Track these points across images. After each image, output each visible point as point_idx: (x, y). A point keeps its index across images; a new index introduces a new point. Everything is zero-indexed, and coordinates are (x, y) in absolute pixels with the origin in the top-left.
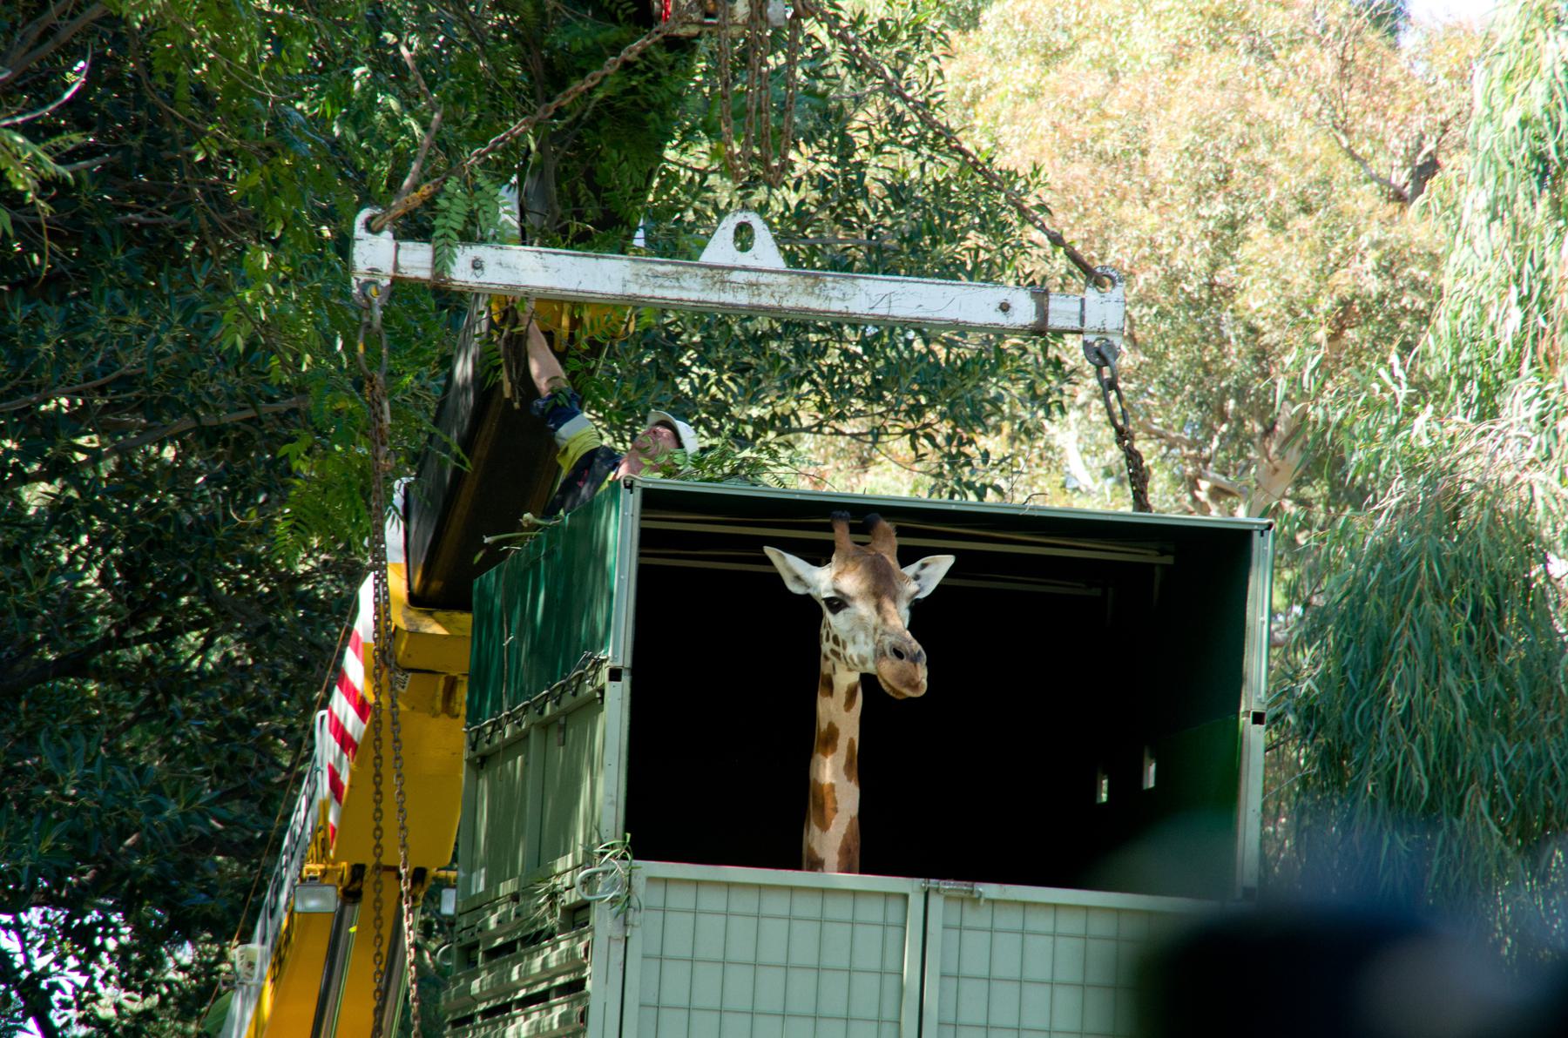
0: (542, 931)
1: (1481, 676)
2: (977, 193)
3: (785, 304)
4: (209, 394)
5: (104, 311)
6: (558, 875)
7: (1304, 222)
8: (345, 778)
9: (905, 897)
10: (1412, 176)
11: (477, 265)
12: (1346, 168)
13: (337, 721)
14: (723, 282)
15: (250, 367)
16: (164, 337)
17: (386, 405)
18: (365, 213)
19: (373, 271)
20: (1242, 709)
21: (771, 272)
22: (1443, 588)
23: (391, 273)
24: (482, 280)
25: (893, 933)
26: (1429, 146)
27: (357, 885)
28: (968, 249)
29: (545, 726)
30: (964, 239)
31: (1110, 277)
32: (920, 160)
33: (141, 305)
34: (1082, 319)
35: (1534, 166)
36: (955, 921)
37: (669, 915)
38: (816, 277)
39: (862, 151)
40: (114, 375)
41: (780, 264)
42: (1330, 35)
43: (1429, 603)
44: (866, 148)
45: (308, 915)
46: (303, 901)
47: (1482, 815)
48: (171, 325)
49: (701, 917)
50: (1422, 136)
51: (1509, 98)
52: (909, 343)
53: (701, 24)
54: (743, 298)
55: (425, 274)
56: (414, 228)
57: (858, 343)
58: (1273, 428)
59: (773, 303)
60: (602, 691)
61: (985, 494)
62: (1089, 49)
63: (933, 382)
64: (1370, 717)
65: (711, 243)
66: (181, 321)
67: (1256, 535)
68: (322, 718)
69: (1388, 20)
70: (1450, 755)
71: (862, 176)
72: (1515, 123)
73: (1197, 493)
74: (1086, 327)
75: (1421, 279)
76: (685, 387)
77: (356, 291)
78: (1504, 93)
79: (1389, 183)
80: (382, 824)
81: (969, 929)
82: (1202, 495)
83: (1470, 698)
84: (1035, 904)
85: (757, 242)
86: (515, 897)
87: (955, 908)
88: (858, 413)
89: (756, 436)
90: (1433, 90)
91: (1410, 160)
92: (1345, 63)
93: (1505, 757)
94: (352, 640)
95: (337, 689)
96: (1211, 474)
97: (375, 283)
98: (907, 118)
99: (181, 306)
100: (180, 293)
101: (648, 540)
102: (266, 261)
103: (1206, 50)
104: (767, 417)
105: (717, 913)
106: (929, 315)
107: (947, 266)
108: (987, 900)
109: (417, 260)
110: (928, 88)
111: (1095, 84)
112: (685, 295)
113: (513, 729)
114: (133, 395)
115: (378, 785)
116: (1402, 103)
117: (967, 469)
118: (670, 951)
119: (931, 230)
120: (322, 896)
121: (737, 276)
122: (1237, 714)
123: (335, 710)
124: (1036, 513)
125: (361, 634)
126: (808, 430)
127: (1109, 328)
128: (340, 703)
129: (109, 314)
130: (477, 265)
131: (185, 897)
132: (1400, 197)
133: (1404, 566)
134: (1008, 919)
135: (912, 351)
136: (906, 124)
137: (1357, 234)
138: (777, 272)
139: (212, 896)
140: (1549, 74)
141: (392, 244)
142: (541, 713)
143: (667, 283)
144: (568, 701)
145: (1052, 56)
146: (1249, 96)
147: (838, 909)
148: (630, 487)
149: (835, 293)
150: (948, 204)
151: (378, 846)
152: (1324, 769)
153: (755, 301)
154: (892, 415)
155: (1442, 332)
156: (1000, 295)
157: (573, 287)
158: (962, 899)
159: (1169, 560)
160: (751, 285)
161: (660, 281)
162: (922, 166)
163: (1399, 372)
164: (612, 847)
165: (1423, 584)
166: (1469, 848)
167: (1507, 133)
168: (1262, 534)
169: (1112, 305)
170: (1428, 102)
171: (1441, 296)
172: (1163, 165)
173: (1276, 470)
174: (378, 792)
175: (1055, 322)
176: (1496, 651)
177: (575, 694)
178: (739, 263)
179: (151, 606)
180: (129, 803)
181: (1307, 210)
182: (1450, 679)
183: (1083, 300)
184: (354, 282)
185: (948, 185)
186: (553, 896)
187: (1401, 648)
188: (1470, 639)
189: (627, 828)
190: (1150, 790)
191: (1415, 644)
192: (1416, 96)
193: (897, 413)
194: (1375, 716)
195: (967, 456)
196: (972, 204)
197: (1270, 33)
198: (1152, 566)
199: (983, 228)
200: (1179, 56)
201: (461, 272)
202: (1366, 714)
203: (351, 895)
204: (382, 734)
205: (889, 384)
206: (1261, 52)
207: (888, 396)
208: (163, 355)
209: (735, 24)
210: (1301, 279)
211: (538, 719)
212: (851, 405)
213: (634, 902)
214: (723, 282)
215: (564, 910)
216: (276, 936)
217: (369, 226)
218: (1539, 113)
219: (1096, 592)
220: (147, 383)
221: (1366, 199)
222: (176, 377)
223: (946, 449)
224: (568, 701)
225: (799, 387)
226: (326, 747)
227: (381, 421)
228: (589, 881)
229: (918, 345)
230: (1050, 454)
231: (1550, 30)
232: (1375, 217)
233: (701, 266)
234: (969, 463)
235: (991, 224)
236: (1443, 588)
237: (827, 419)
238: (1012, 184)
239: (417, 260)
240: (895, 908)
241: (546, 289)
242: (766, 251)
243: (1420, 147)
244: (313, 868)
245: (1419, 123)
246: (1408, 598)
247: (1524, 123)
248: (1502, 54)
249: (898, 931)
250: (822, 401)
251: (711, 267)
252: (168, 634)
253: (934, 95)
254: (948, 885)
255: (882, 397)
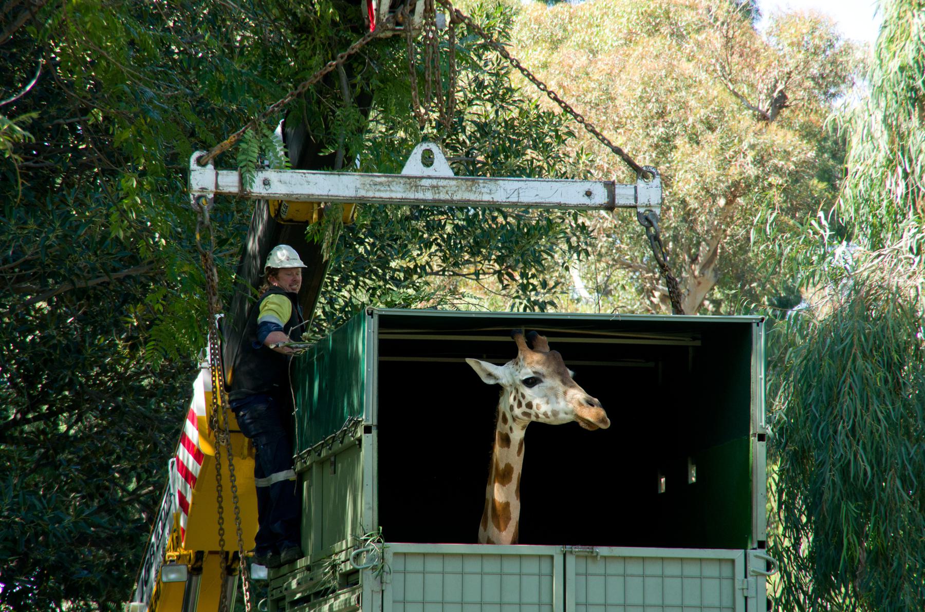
0: (329, 588)
1: (893, 404)
2: (530, 127)
3: (455, 198)
4: (80, 269)
5: (13, 222)
6: (337, 554)
7: (711, 136)
8: (189, 499)
9: (552, 557)
10: (771, 104)
11: (266, 183)
12: (732, 103)
13: (182, 463)
14: (416, 186)
15: (103, 251)
16: (50, 236)
17: (215, 270)
18: (196, 154)
19: (203, 189)
20: (751, 432)
21: (445, 178)
22: (868, 352)
23: (214, 190)
24: (269, 191)
25: (545, 580)
26: (780, 87)
27: (199, 564)
28: (527, 160)
29: (322, 463)
30: (525, 154)
31: (651, 172)
32: (495, 108)
33: (35, 217)
34: (636, 199)
35: (909, 95)
36: (583, 571)
37: (408, 575)
38: (473, 180)
39: (461, 105)
40: (21, 260)
41: (451, 174)
42: (719, 23)
43: (860, 362)
44: (463, 103)
45: (169, 583)
46: (167, 575)
47: (898, 489)
48: (54, 229)
49: (427, 576)
50: (777, 81)
51: (892, 53)
52: (494, 219)
53: (394, 30)
54: (429, 196)
55: (235, 189)
56: (222, 163)
57: (464, 220)
58: (696, 258)
59: (448, 197)
60: (360, 440)
61: (545, 308)
62: (576, 38)
63: (511, 241)
64: (828, 432)
65: (408, 163)
66: (60, 226)
67: (754, 325)
68: (173, 463)
69: (749, 12)
70: (878, 454)
71: (462, 120)
72: (896, 69)
73: (652, 299)
74: (639, 203)
75: (780, 166)
76: (361, 250)
77: (193, 202)
78: (889, 52)
79: (757, 109)
80: (223, 526)
81: (592, 575)
82: (656, 300)
83: (888, 417)
84: (631, 558)
85: (435, 161)
86: (308, 568)
87: (582, 562)
88: (468, 262)
89: (406, 279)
90: (781, 53)
91: (769, 95)
92: (728, 40)
93: (909, 454)
94: (190, 415)
95: (181, 445)
96: (660, 287)
97: (205, 197)
98: (486, 83)
99: (60, 216)
100: (57, 208)
101: (384, 347)
102: (135, 183)
103: (646, 36)
104: (412, 267)
105: (488, 574)
106: (543, 201)
107: (515, 171)
108: (602, 557)
109: (229, 181)
110: (498, 65)
111: (583, 59)
112: (394, 195)
113: (302, 464)
114: (31, 272)
115: (220, 502)
116: (764, 63)
117: (533, 293)
118: (409, 598)
119: (505, 150)
120: (178, 571)
121: (425, 182)
122: (748, 436)
123: (181, 458)
124: (620, 319)
125: (195, 411)
126: (437, 273)
127: (652, 203)
128: (183, 453)
129: (16, 224)
130: (266, 183)
131: (73, 573)
132: (763, 117)
133: (842, 340)
134: (615, 568)
135: (497, 224)
136: (486, 87)
137: (741, 141)
138: (449, 178)
139: (90, 572)
140: (916, 38)
141: (214, 172)
142: (319, 455)
143: (382, 188)
144: (338, 446)
145: (555, 44)
146: (675, 63)
147: (511, 566)
148: (371, 314)
149: (485, 190)
150: (514, 134)
151: (222, 540)
152: (793, 465)
153: (436, 197)
154: (487, 262)
155: (848, 197)
156: (587, 186)
157: (326, 193)
158: (586, 557)
159: (698, 343)
160: (433, 187)
161: (378, 187)
162: (497, 112)
163: (824, 222)
164: (371, 535)
165: (856, 350)
166: (891, 510)
167: (892, 75)
168: (758, 325)
169: (654, 189)
170: (779, 61)
171: (846, 174)
172: (624, 106)
173: (699, 283)
174: (221, 507)
175: (619, 201)
176: (900, 389)
177: (342, 442)
178: (425, 174)
179: (43, 397)
180: (41, 518)
181: (711, 128)
182: (875, 405)
183: (636, 188)
184: (191, 196)
185: (513, 122)
186: (334, 567)
187: (846, 389)
188: (886, 381)
189: (379, 524)
190: (693, 484)
191: (853, 385)
192: (772, 58)
193: (489, 261)
194: (831, 432)
195: (532, 284)
196: (527, 133)
197: (684, 24)
198: (687, 347)
199: (535, 147)
200: (630, 39)
201: (257, 189)
202: (825, 431)
203: (196, 570)
204: (222, 472)
205: (484, 244)
206: (678, 35)
207: (484, 251)
208: (50, 246)
209: (414, 29)
210: (712, 172)
211: (317, 459)
212: (462, 257)
213: (386, 568)
214: (416, 186)
215: (340, 574)
216: (149, 597)
217: (199, 162)
218: (911, 63)
219: (651, 364)
220: (41, 263)
221: (746, 120)
222: (59, 260)
223: (521, 281)
224: (338, 446)
225: (430, 248)
226: (176, 482)
227: (212, 280)
228: (358, 556)
229: (501, 219)
230: (563, 280)
231: (915, 11)
232: (751, 131)
233: (402, 177)
234: (534, 289)
235: (539, 144)
236: (868, 352)
237: (448, 266)
238: (551, 120)
239: (229, 181)
240: (726, 570)
241: (309, 195)
242: (442, 166)
243: (775, 86)
244: (172, 554)
245: (775, 73)
246: (848, 358)
247: (902, 69)
248: (885, 27)
249: (548, 578)
250: (445, 256)
251: (409, 178)
252: (52, 417)
253: (502, 69)
254: (577, 549)
255: (480, 252)
